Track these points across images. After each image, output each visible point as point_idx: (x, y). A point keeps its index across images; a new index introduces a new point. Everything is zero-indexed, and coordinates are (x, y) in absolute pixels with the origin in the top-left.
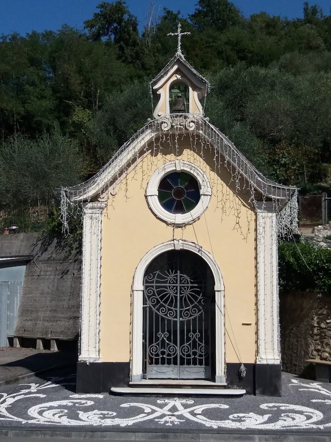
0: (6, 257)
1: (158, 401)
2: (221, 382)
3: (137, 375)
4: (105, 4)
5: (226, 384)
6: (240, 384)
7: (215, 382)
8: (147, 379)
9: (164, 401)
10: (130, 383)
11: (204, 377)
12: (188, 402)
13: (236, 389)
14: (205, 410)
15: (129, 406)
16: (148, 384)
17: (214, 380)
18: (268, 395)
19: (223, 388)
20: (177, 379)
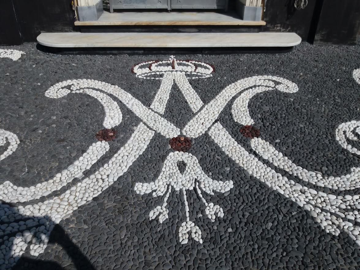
0: (285, 43)
1: (136, 70)
2: (254, 19)
3: (89, 7)
4: (15, 250)
5: (263, 23)
6: (288, 23)
7: (241, 17)
8: (112, 10)
9: (150, 67)
10: (77, 23)
11: (215, 7)
12: (199, 70)
13: (279, 31)
14: (337, 175)
15: (66, 92)
16: (112, 24)
17: (240, 16)
18: (335, 43)
19: (256, 30)
20: (165, 10)
